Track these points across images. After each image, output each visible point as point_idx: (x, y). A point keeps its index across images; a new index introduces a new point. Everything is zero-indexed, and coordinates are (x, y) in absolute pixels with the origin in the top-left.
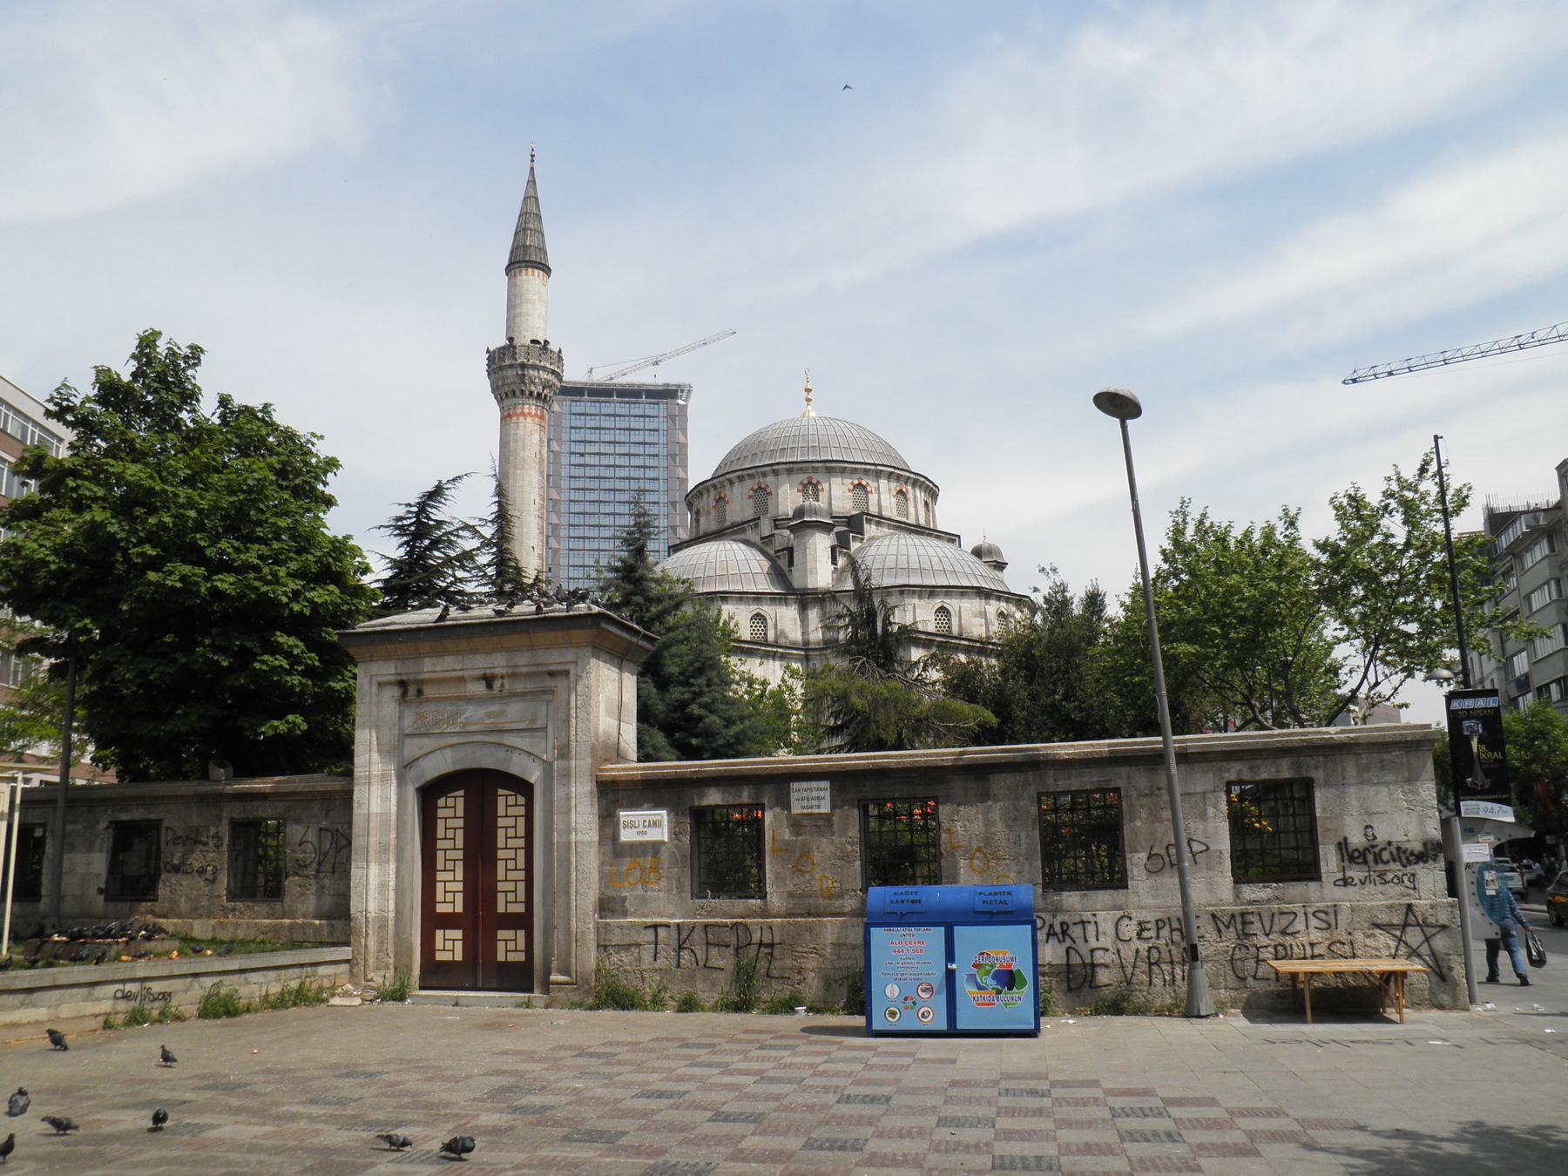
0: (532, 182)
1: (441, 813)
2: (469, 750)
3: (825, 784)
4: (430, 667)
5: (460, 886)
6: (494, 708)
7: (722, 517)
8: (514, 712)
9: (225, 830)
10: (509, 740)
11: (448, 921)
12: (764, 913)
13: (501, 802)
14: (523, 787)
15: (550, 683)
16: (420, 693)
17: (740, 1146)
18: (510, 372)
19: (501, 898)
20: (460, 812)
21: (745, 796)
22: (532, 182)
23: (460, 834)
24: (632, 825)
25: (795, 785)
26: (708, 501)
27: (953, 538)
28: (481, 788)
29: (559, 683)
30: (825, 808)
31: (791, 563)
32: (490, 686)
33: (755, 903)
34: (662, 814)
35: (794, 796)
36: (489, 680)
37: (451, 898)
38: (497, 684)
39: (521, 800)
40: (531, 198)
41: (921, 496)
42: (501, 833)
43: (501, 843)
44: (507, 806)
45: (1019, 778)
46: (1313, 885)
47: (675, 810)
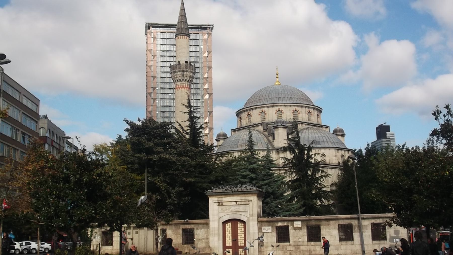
1: (226, 227)
3: (300, 222)
4: (225, 199)
6: (237, 207)
7: (250, 121)
8: (241, 208)
9: (181, 232)
10: (240, 213)
11: (229, 247)
12: (290, 245)
13: (239, 225)
14: (244, 222)
15: (248, 203)
17: (330, 179)
18: (179, 73)
19: (239, 243)
20: (231, 227)
21: (286, 224)
23: (231, 231)
24: (265, 229)
25: (295, 222)
26: (244, 115)
27: (327, 127)
28: (235, 221)
29: (250, 203)
30: (300, 226)
31: (274, 139)
33: (288, 243)
34: (270, 227)
35: (295, 224)
36: (236, 202)
37: (229, 243)
38: (238, 203)
40: (183, 10)
41: (316, 112)
43: (239, 232)
45: (335, 221)
46: (385, 241)
47: (273, 227)
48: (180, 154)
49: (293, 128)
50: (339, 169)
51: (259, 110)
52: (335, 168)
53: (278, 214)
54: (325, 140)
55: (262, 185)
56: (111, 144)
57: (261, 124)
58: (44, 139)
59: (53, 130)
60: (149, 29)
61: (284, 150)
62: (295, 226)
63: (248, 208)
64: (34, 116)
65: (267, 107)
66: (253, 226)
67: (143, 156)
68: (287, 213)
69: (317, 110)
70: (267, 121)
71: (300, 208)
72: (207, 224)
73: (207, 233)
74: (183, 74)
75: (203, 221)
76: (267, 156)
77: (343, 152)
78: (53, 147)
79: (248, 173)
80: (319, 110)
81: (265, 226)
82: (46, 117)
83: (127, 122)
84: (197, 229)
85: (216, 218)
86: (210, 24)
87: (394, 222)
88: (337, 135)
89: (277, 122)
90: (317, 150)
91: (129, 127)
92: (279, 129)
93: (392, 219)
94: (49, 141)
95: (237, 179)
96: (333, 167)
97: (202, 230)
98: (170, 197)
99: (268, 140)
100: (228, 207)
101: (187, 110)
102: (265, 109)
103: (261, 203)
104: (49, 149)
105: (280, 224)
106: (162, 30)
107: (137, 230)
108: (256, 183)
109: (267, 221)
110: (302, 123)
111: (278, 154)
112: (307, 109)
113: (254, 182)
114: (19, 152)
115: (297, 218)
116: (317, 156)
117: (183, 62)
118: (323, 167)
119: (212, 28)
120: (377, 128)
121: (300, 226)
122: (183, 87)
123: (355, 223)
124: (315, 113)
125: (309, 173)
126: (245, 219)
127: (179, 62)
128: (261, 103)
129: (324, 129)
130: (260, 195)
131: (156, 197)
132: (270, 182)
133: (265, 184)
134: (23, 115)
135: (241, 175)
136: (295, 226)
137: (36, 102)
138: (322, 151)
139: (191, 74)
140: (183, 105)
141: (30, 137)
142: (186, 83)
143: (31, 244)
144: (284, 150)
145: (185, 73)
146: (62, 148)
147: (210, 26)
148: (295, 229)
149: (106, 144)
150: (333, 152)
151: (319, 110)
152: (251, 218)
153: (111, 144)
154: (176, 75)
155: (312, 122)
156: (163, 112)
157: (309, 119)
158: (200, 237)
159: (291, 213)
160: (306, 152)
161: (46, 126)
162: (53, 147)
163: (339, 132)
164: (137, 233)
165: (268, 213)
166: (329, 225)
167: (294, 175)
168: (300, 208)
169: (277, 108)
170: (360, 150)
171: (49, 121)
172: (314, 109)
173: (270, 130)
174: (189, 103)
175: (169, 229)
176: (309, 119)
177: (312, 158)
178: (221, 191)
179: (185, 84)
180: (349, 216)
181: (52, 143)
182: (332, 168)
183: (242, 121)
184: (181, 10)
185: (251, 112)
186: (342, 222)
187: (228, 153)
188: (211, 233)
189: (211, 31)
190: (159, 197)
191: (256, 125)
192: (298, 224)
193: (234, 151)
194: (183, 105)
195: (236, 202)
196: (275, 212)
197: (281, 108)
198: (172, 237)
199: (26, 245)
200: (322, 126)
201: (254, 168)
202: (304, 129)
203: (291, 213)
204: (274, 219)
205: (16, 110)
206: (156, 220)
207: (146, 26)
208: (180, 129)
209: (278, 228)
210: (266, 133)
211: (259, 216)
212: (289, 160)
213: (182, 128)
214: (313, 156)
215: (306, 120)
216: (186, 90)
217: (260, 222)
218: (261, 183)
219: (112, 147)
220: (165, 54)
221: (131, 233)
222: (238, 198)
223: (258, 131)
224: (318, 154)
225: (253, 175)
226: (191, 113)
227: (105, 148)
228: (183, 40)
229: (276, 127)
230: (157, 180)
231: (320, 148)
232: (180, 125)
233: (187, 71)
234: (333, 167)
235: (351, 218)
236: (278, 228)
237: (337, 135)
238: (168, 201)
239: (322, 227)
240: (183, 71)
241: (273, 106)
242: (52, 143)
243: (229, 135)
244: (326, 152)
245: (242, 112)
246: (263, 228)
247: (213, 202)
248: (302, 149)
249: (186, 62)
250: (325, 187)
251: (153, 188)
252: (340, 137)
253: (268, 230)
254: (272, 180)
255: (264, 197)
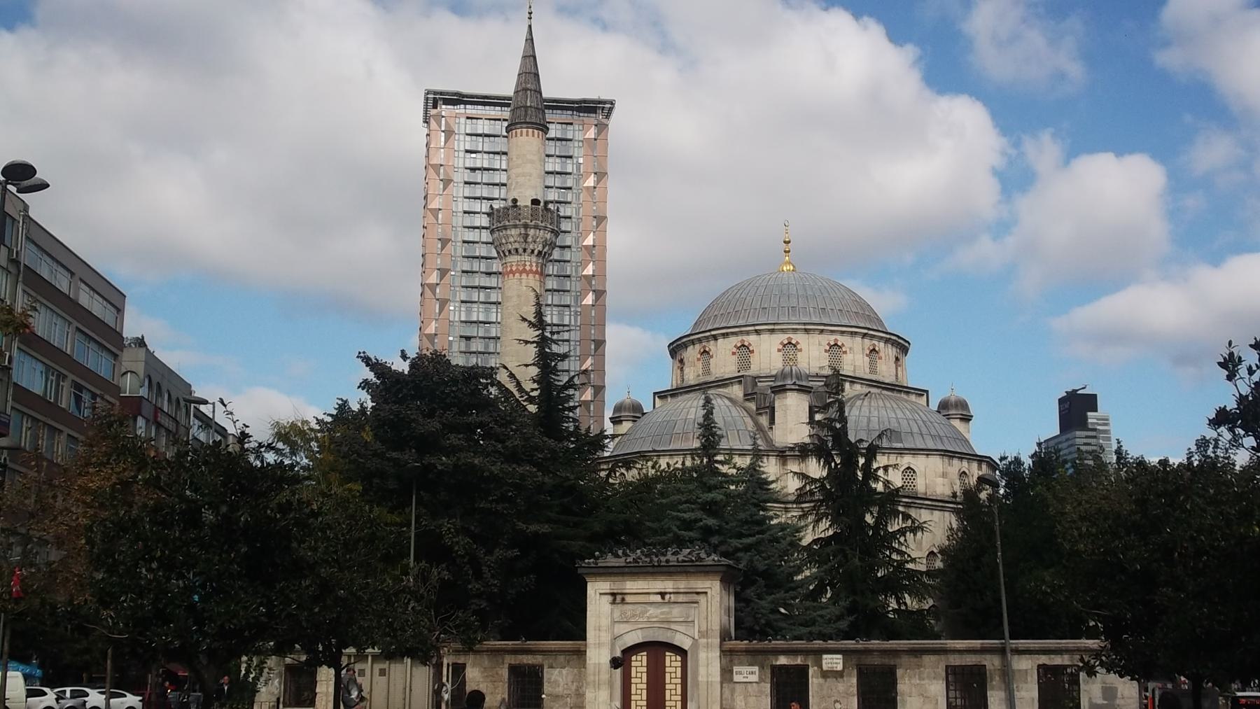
0: (530, 40)
2: (651, 631)
3: (840, 656)
4: (631, 585)
5: (633, 697)
6: (665, 609)
7: (707, 371)
8: (676, 612)
9: (505, 673)
13: (668, 659)
15: (695, 597)
16: (623, 599)
17: (928, 539)
18: (514, 232)
21: (799, 661)
22: (530, 40)
23: (645, 675)
24: (740, 673)
26: (692, 353)
27: (922, 393)
28: (656, 649)
29: (702, 599)
30: (840, 667)
31: (772, 421)
32: (663, 598)
34: (756, 669)
36: (663, 594)
38: (667, 597)
39: (679, 658)
42: (668, 675)
44: (672, 663)
47: (762, 667)
48: (513, 457)
49: (829, 393)
50: (955, 511)
51: (735, 341)
52: (942, 509)
53: (777, 633)
54: (915, 430)
55: (737, 550)
56: (319, 422)
57: (739, 380)
58: (134, 406)
59: (162, 380)
60: (435, 107)
61: (803, 452)
62: (825, 667)
63: (693, 612)
64: (109, 338)
65: (758, 332)
66: (708, 664)
67: (409, 457)
68: (804, 630)
69: (894, 343)
70: (754, 370)
71: (839, 618)
72: (581, 654)
73: (580, 679)
74: (527, 235)
75: (568, 644)
76: (753, 470)
77: (965, 463)
78: (159, 426)
79: (699, 514)
80: (902, 347)
81: (741, 664)
82: (141, 342)
83: (367, 360)
84: (551, 667)
85: (606, 637)
86: (603, 97)
87: (1102, 664)
88: (948, 417)
89: (783, 375)
90: (893, 457)
91: (371, 376)
92: (789, 394)
93: (1097, 654)
94: (147, 409)
95: (669, 530)
96: (936, 504)
97: (564, 671)
98: (478, 575)
99: (756, 423)
100: (639, 608)
101: (532, 334)
102: (752, 339)
103: (732, 599)
104: (148, 429)
105: (783, 660)
106: (471, 110)
107: (385, 665)
108: (721, 543)
109: (747, 652)
110: (854, 380)
111: (784, 464)
112: (867, 341)
113: (715, 540)
114: (63, 437)
115: (831, 644)
116: (891, 472)
117: (525, 202)
118: (908, 505)
119: (611, 110)
120: (1061, 401)
121: (840, 667)
122: (524, 271)
123: (992, 663)
124: (888, 352)
125: (869, 519)
126: (686, 644)
127: (515, 201)
128: (741, 322)
129: (913, 398)
130: (729, 578)
131: (439, 573)
132: (759, 543)
133: (747, 548)
134: (78, 336)
135: (679, 519)
136: (825, 667)
137: (116, 299)
138: (907, 460)
139: (548, 236)
140: (524, 319)
141: (94, 396)
142: (534, 259)
143: (87, 695)
144: (803, 452)
145: (532, 232)
146: (182, 430)
147: (605, 102)
148: (825, 675)
149: (307, 422)
150: (936, 462)
151: (902, 347)
152: (703, 641)
153: (319, 422)
154: (507, 237)
155: (881, 379)
156: (468, 338)
157: (873, 370)
158: (559, 690)
159: (815, 629)
160: (862, 461)
161: (140, 368)
162: (159, 426)
163: (956, 409)
164: (382, 672)
165: (749, 631)
166: (919, 666)
167: (824, 524)
168: (839, 618)
169: (783, 338)
170: (1017, 461)
171: (150, 355)
172: (887, 341)
173: (762, 396)
174: (539, 314)
175: (474, 666)
176: (873, 370)
177: (877, 479)
178: (620, 562)
179: (531, 262)
180: (977, 643)
181: (156, 417)
182: (932, 508)
183: (686, 370)
184: (524, 57)
185: (711, 345)
186: (956, 660)
187: (643, 456)
188: (591, 678)
189: (608, 117)
190: (446, 575)
191: (724, 383)
192: (833, 662)
193: (660, 453)
194: (524, 319)
195: (663, 594)
196: (768, 624)
197: (795, 338)
198: (483, 688)
199: (72, 697)
200: (908, 390)
201: (714, 502)
202: (858, 397)
203: (815, 629)
204: (765, 644)
205: (59, 321)
206: (438, 639)
207: (427, 99)
208: (511, 387)
209: (777, 672)
210: (752, 406)
211: (725, 636)
212: (814, 481)
213: (518, 384)
214: (881, 473)
215: (864, 372)
216: (533, 281)
217: (729, 656)
218: (735, 543)
219: (321, 431)
220: (478, 177)
221: (368, 672)
222: (667, 585)
223: (730, 399)
224: (895, 466)
225: (711, 522)
226: (543, 342)
227: (301, 433)
228: (527, 141)
229: (780, 390)
230: (446, 525)
231: (901, 452)
232: (512, 376)
233: (536, 227)
234: (936, 504)
235: (983, 651)
236: (777, 672)
237: (948, 417)
238: (474, 586)
239: (899, 672)
240: (526, 226)
241: (772, 331)
242: (156, 417)
243: (647, 408)
244: (918, 463)
245: (685, 346)
246: (735, 669)
247: (597, 593)
248: (849, 451)
249: (535, 202)
250: (913, 560)
251: (432, 549)
252: (957, 423)
253: (747, 673)
254: (766, 536)
255: (740, 583)
